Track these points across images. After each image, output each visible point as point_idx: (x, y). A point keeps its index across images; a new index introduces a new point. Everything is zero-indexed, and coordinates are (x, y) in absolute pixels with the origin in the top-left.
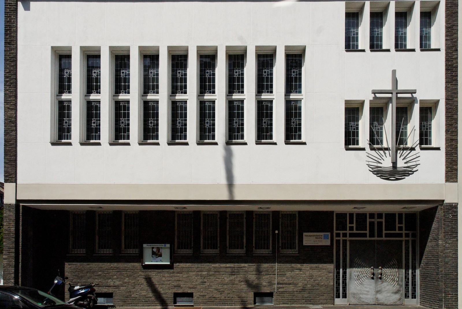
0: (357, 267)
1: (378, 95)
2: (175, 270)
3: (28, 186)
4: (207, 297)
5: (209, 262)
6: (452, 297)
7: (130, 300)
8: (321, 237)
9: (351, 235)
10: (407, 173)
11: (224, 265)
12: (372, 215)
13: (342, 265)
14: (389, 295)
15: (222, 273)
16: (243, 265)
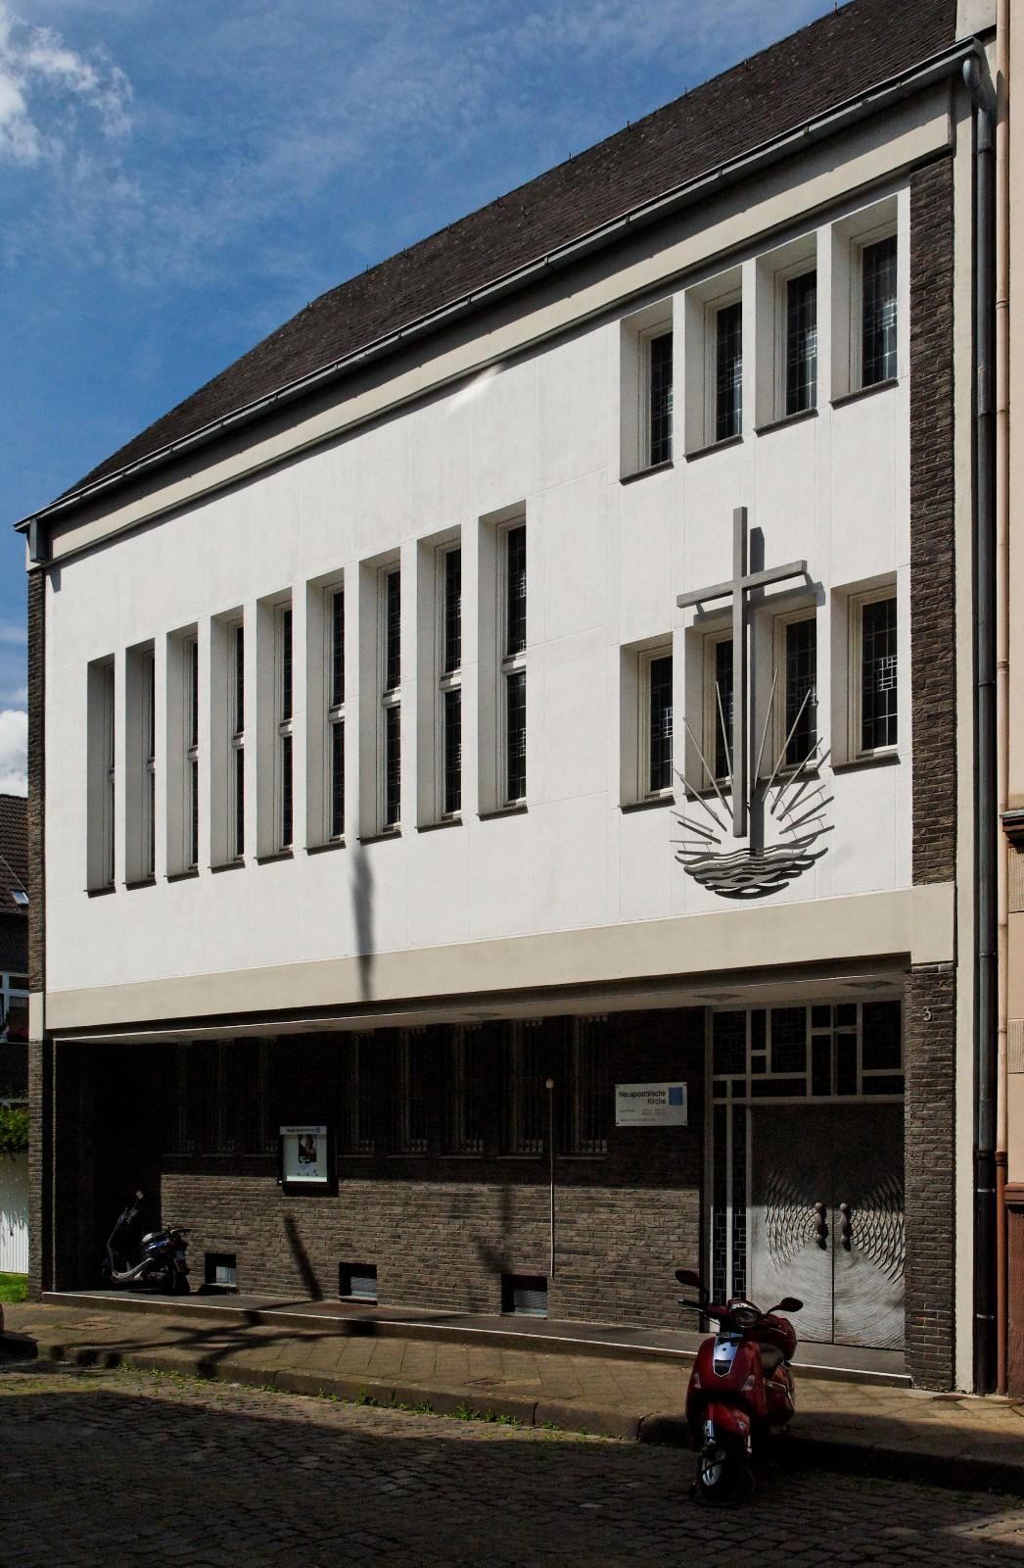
0: (773, 1204)
1: (708, 607)
2: (344, 1199)
3: (71, 997)
4: (403, 1279)
5: (407, 1178)
6: (932, 1324)
7: (263, 1275)
8: (662, 1098)
9: (760, 1088)
10: (789, 868)
11: (435, 1187)
12: (821, 1015)
13: (728, 1195)
14: (875, 1309)
15: (434, 1210)
16: (477, 1188)
